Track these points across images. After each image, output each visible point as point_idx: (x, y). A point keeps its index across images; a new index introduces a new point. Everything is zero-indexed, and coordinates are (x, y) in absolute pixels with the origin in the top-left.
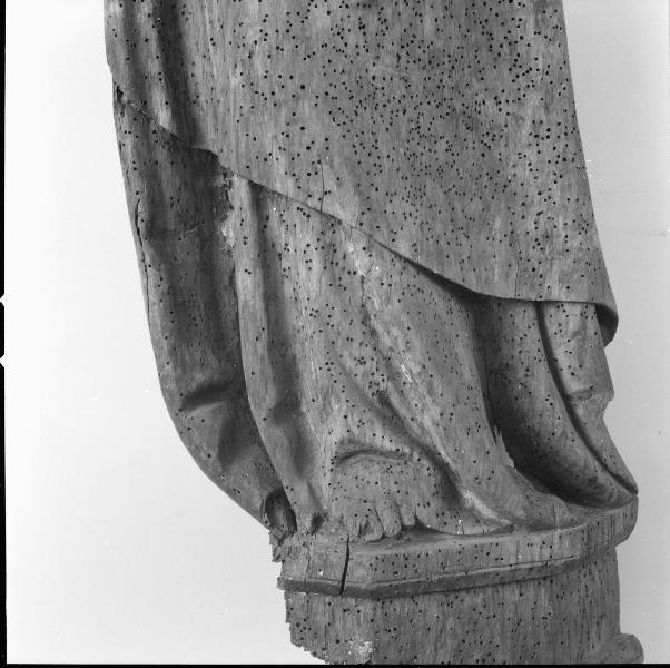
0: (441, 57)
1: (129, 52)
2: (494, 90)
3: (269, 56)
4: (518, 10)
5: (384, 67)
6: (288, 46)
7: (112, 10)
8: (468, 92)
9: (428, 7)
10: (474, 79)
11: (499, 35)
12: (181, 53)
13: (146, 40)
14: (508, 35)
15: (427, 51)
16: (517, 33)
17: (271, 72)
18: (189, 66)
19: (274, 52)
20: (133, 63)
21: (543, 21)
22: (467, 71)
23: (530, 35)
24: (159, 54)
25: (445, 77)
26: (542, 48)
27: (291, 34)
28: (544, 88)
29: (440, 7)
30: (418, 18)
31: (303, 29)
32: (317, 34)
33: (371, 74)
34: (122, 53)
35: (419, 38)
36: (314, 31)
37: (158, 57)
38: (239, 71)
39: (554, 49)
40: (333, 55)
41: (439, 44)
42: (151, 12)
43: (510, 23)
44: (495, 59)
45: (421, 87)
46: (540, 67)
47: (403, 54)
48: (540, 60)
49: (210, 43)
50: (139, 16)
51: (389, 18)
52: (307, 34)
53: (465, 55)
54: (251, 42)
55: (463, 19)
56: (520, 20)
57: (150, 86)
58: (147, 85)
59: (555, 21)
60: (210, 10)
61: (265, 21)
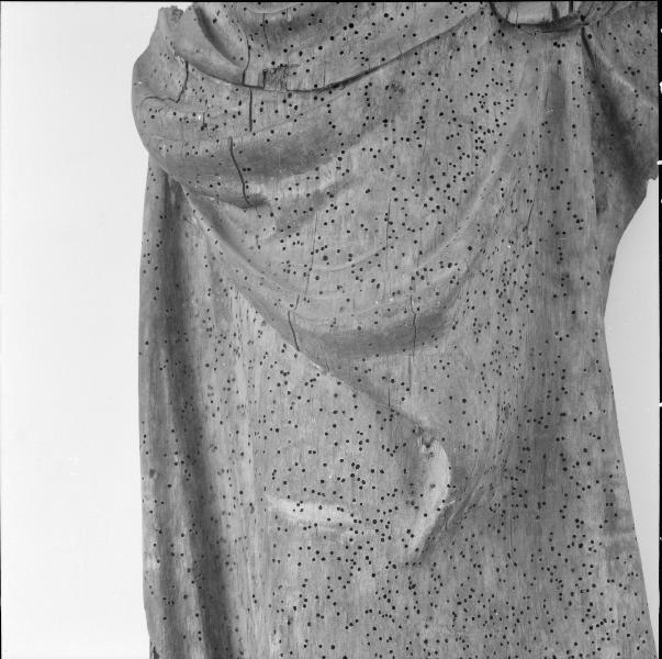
0: (504, 611)
1: (166, 610)
2: (566, 642)
3: (309, 624)
4: (589, 555)
5: (439, 627)
6: (329, 613)
7: (149, 566)
8: (537, 647)
9: (488, 557)
10: (542, 632)
11: (570, 582)
12: (223, 606)
13: (185, 597)
14: (579, 582)
15: (488, 605)
16: (588, 581)
17: (311, 642)
18: (234, 620)
19: (314, 620)
20: (171, 620)
21: (616, 568)
22: (534, 623)
23: (603, 583)
24: (198, 612)
25: (509, 632)
26: (617, 596)
27: (332, 600)
28: (621, 641)
29: (502, 556)
30: (477, 570)
31: (345, 596)
32: (361, 598)
33: (423, 638)
34: (159, 613)
35: (478, 592)
36: (357, 595)
37: (197, 615)
38: (278, 637)
39: (630, 599)
40: (376, 620)
41: (502, 596)
42: (190, 567)
43: (582, 569)
44: (566, 609)
45: (481, 646)
46: (615, 618)
47: (460, 612)
48: (615, 610)
49: (252, 600)
50: (177, 571)
51: (443, 574)
52: (350, 599)
53: (532, 606)
54: (291, 607)
55: (528, 565)
56: (592, 566)
57: (189, 647)
58: (185, 646)
59: (630, 567)
60: (253, 565)
61: (304, 586)
